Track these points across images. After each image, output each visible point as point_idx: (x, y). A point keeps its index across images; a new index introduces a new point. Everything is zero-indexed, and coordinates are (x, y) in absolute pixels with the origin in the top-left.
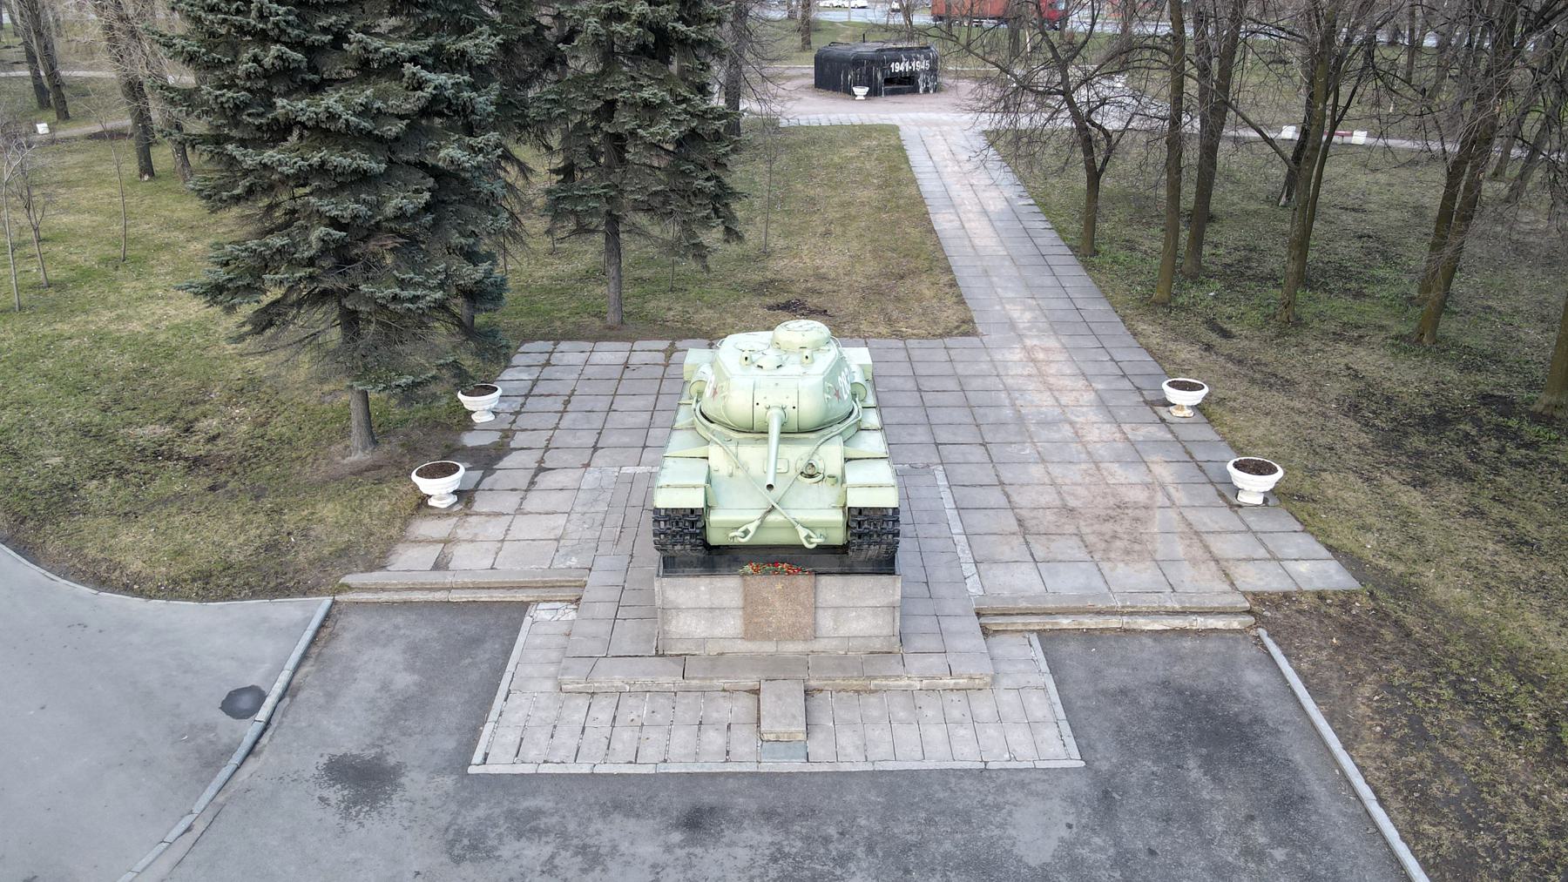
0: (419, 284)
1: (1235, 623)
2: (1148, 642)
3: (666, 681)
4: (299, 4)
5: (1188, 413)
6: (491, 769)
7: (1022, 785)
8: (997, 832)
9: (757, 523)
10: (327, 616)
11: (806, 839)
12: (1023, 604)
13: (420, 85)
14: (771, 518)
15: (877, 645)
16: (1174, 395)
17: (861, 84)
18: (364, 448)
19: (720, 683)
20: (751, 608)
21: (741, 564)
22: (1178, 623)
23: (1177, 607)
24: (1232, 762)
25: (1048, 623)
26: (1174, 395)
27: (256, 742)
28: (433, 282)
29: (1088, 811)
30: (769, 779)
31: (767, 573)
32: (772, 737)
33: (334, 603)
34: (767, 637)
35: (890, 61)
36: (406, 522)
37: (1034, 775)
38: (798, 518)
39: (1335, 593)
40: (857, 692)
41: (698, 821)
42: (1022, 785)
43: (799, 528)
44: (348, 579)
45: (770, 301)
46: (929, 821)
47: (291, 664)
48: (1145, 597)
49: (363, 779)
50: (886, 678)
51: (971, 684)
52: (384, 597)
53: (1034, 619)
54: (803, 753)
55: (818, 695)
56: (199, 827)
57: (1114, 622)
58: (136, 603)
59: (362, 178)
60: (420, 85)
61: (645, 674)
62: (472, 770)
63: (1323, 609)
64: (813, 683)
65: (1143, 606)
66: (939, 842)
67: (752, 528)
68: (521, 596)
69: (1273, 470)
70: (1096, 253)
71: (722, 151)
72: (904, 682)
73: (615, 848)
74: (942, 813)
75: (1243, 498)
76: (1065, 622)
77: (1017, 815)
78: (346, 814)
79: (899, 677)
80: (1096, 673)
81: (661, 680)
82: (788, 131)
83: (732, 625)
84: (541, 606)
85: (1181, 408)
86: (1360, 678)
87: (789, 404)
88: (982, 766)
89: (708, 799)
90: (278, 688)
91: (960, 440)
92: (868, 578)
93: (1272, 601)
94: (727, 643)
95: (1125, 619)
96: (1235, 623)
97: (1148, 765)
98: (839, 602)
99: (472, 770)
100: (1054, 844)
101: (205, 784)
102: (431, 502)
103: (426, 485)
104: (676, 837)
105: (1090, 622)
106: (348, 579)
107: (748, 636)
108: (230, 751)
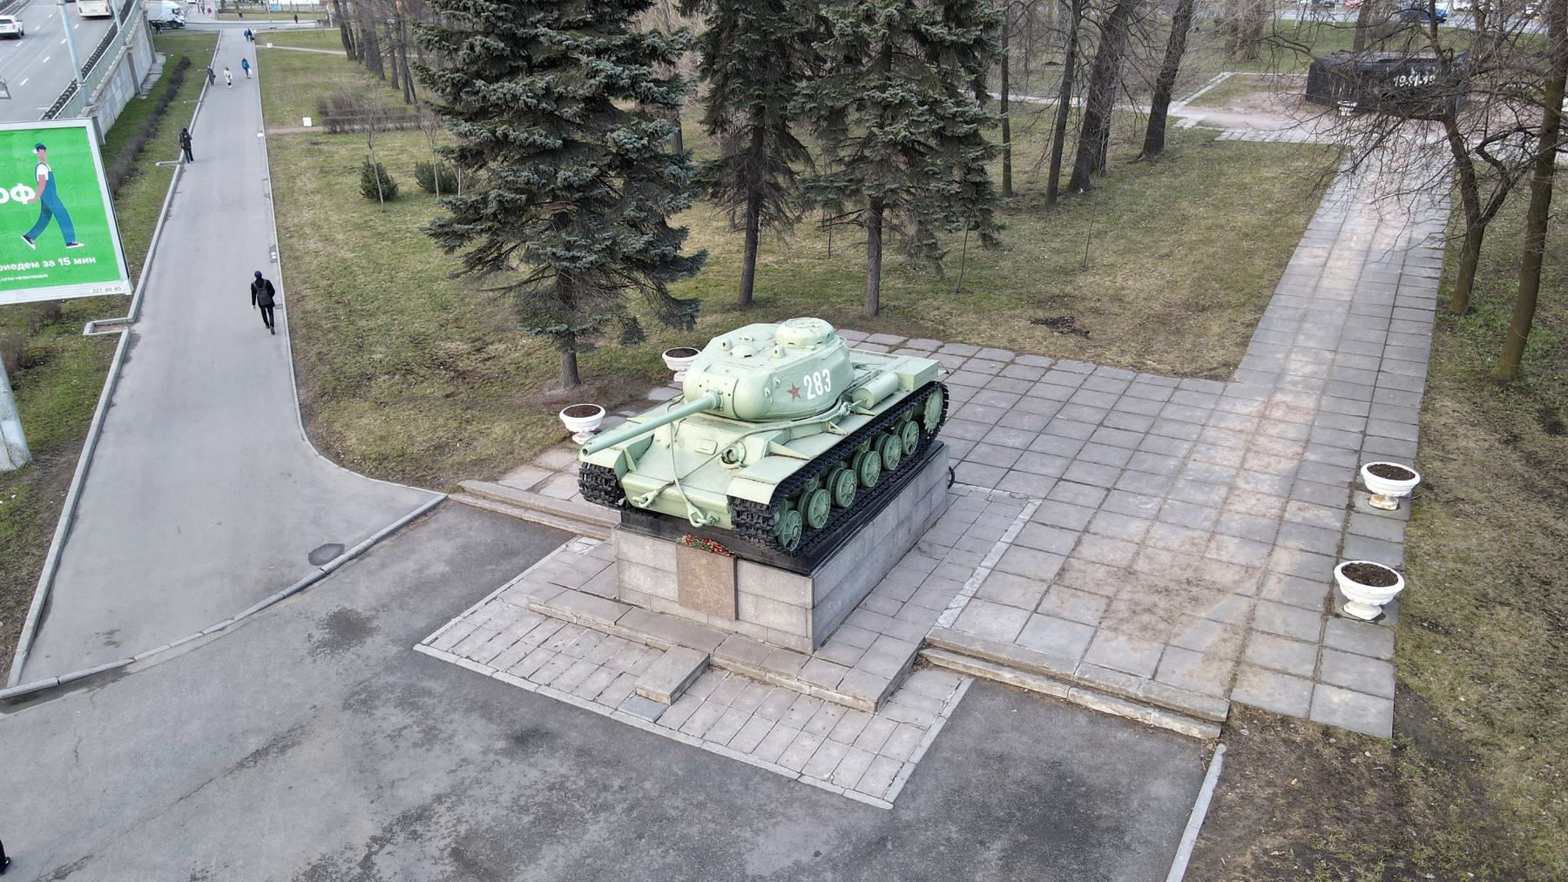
0: (581, 247)
1: (1195, 731)
2: (1082, 720)
3: (605, 623)
4: (520, 4)
5: (1387, 504)
6: (430, 651)
7: (814, 805)
8: (748, 835)
9: (655, 493)
10: (434, 507)
11: (591, 782)
12: (978, 647)
13: (594, 73)
14: (669, 491)
15: (793, 643)
16: (1373, 482)
17: (1350, 97)
18: (567, 385)
19: (644, 637)
20: (684, 574)
21: (681, 533)
22: (1129, 711)
23: (1140, 695)
24: (1043, 858)
25: (990, 672)
26: (1373, 482)
27: (310, 584)
28: (597, 247)
29: (849, 848)
30: (609, 725)
31: (696, 547)
32: (643, 693)
33: (446, 499)
34: (696, 607)
35: (1392, 74)
36: (544, 450)
37: (834, 801)
38: (691, 496)
39: (1349, 733)
40: (753, 679)
41: (524, 740)
42: (814, 805)
43: (689, 506)
44: (466, 484)
45: (1040, 314)
46: (701, 806)
47: (375, 537)
48: (1109, 674)
49: (347, 629)
50: (781, 674)
51: (855, 703)
52: (480, 503)
53: (977, 665)
54: (656, 714)
55: (718, 672)
56: (228, 630)
57: (1059, 691)
58: (331, 467)
59: (543, 152)
60: (594, 73)
61: (591, 612)
62: (418, 648)
63: (1319, 746)
64: (717, 660)
65: (1100, 682)
66: (690, 824)
67: (650, 496)
68: (571, 528)
69: (1391, 580)
70: (1472, 310)
71: (972, 155)
72: (794, 683)
73: (451, 737)
74: (719, 802)
75: (1350, 609)
76: (1007, 676)
77: (780, 829)
78: (313, 652)
79: (789, 677)
80: (995, 732)
81: (599, 620)
82: (1229, 143)
83: (670, 588)
84: (584, 540)
85: (1382, 498)
86: (1280, 827)
87: (727, 390)
88: (795, 776)
89: (552, 725)
90: (353, 551)
91: (1090, 480)
92: (782, 573)
93: (1262, 721)
94: (668, 604)
95: (1073, 691)
96: (1195, 731)
97: (953, 831)
98: (758, 590)
99: (418, 648)
100: (788, 862)
101: (256, 601)
102: (575, 438)
103: (571, 423)
104: (501, 744)
105: (1033, 683)
106: (466, 484)
107: (683, 603)
108: (289, 585)
